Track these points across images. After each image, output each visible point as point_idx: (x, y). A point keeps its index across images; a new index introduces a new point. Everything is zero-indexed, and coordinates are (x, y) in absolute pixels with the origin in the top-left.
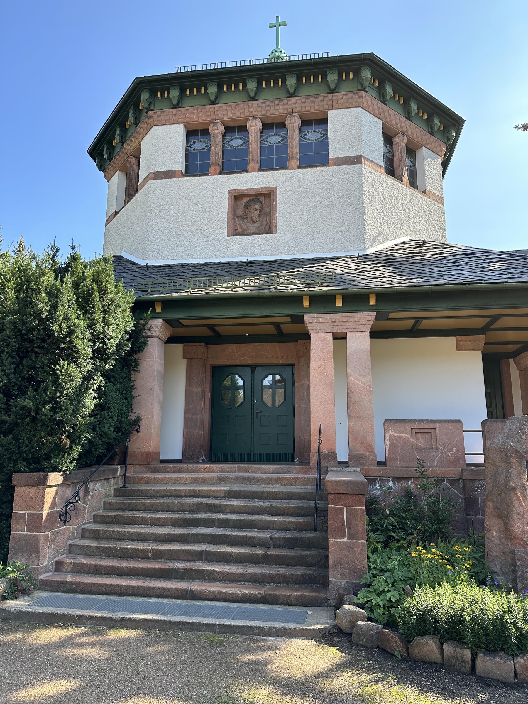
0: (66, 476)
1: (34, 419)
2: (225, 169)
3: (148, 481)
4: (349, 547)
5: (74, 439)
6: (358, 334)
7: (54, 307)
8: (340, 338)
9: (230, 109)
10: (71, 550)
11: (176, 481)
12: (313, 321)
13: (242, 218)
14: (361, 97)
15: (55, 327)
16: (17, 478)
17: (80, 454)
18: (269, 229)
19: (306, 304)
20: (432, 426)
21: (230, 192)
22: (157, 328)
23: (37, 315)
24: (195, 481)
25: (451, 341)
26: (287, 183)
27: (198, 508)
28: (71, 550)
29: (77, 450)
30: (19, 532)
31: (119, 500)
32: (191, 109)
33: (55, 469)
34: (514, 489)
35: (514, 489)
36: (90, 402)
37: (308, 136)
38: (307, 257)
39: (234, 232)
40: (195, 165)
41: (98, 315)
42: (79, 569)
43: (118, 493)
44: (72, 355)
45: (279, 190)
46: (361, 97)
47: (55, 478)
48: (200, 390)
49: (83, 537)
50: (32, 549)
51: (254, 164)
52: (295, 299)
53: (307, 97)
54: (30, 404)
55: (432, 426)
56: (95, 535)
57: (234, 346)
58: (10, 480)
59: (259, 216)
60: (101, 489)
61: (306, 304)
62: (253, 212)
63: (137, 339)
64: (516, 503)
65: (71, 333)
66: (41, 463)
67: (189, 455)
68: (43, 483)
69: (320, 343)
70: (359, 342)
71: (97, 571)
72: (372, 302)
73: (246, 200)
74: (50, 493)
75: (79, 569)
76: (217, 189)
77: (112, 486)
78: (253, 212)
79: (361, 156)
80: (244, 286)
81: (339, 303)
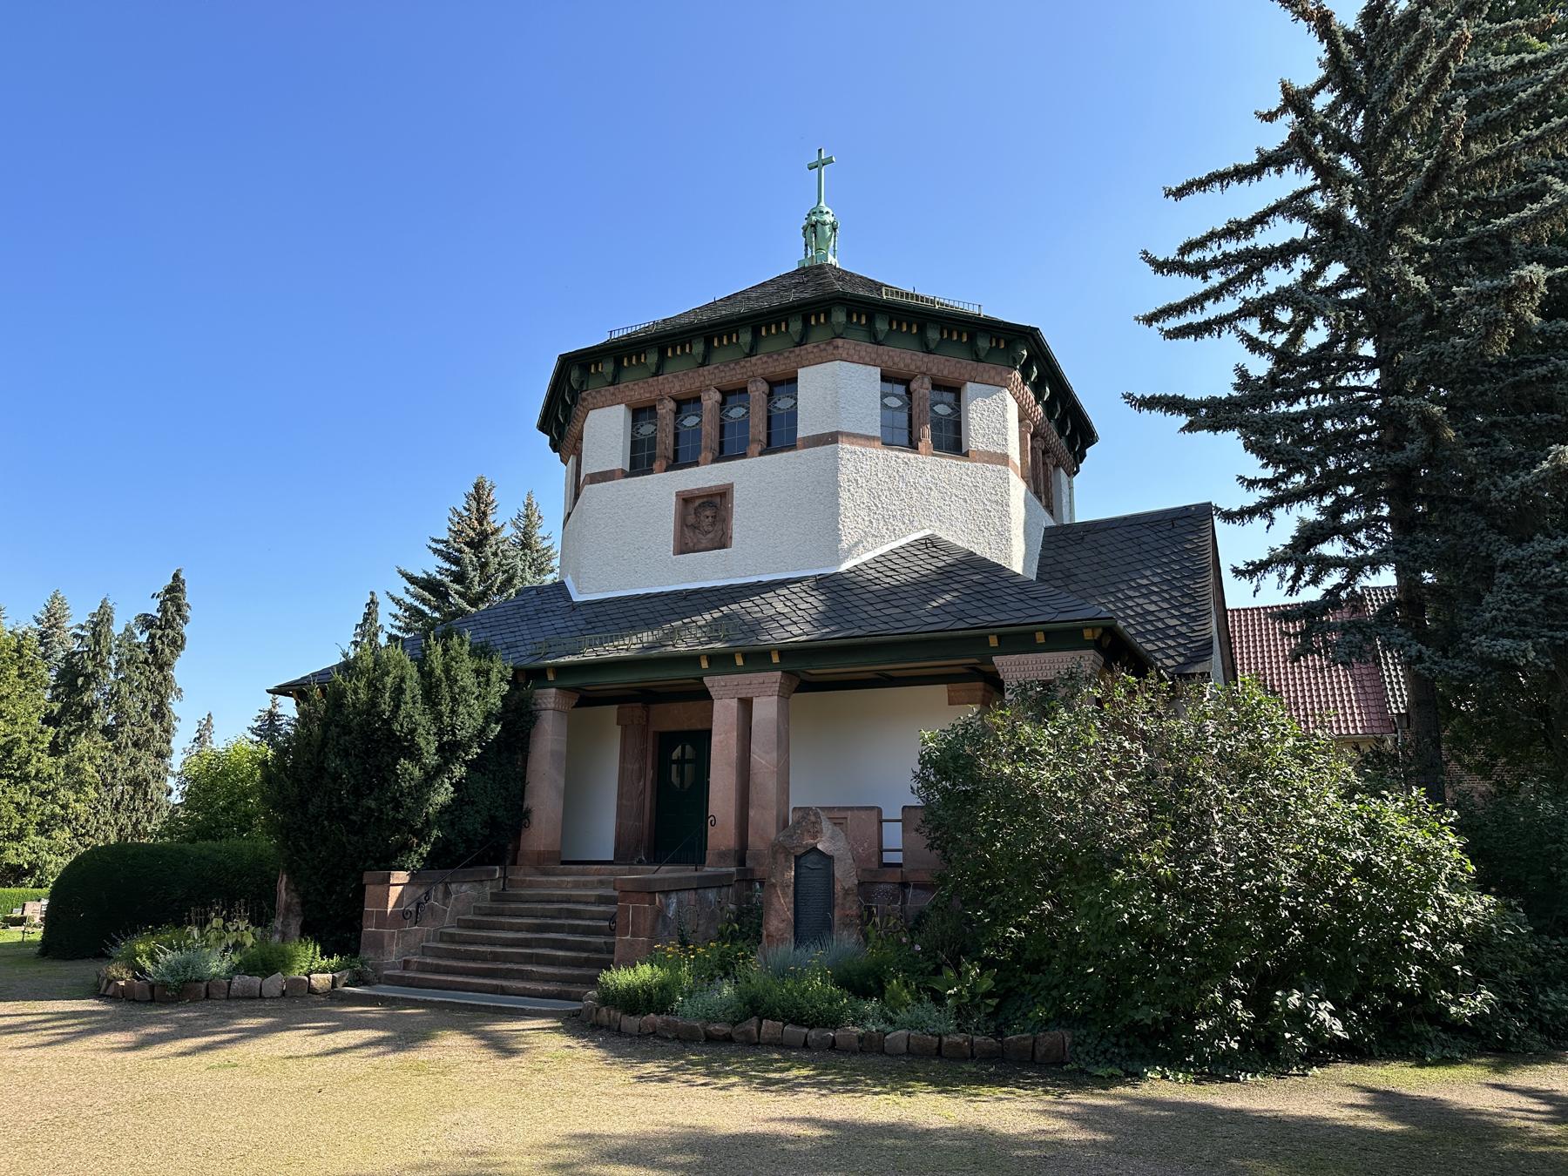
0: (413, 876)
1: (379, 819)
2: (676, 463)
3: (531, 885)
4: (631, 944)
5: (422, 836)
6: (765, 699)
7: (397, 707)
8: (746, 705)
9: (676, 382)
10: (424, 951)
11: (558, 886)
12: (713, 683)
13: (694, 527)
14: (837, 347)
15: (396, 727)
16: (367, 877)
17: (429, 853)
18: (723, 543)
19: (705, 665)
20: (843, 814)
21: (678, 494)
22: (549, 698)
23: (380, 715)
24: (576, 885)
25: (942, 689)
26: (748, 477)
27: (560, 914)
28: (424, 951)
29: (425, 849)
30: (369, 929)
31: (495, 905)
32: (631, 385)
33: (402, 868)
34: (774, 886)
35: (774, 886)
36: (443, 794)
37: (778, 405)
38: (766, 578)
39: (682, 548)
40: (641, 461)
41: (444, 708)
42: (423, 968)
43: (496, 897)
44: (413, 753)
45: (736, 487)
46: (837, 347)
47: (400, 877)
48: (636, 766)
49: (441, 941)
50: (378, 944)
51: (706, 455)
52: (691, 660)
53: (769, 355)
54: (373, 805)
55: (843, 814)
56: (452, 939)
57: (680, 705)
58: (361, 879)
59: (713, 524)
60: (467, 893)
61: (705, 665)
62: (704, 520)
63: (517, 721)
64: (775, 900)
65: (412, 731)
66: (388, 861)
67: (624, 854)
68: (386, 882)
69: (724, 714)
70: (766, 709)
71: (437, 970)
72: (776, 659)
73: (697, 503)
74: (394, 893)
75: (423, 968)
76: (663, 489)
77: (488, 889)
78: (704, 520)
79: (837, 433)
80: (629, 646)
81: (740, 662)
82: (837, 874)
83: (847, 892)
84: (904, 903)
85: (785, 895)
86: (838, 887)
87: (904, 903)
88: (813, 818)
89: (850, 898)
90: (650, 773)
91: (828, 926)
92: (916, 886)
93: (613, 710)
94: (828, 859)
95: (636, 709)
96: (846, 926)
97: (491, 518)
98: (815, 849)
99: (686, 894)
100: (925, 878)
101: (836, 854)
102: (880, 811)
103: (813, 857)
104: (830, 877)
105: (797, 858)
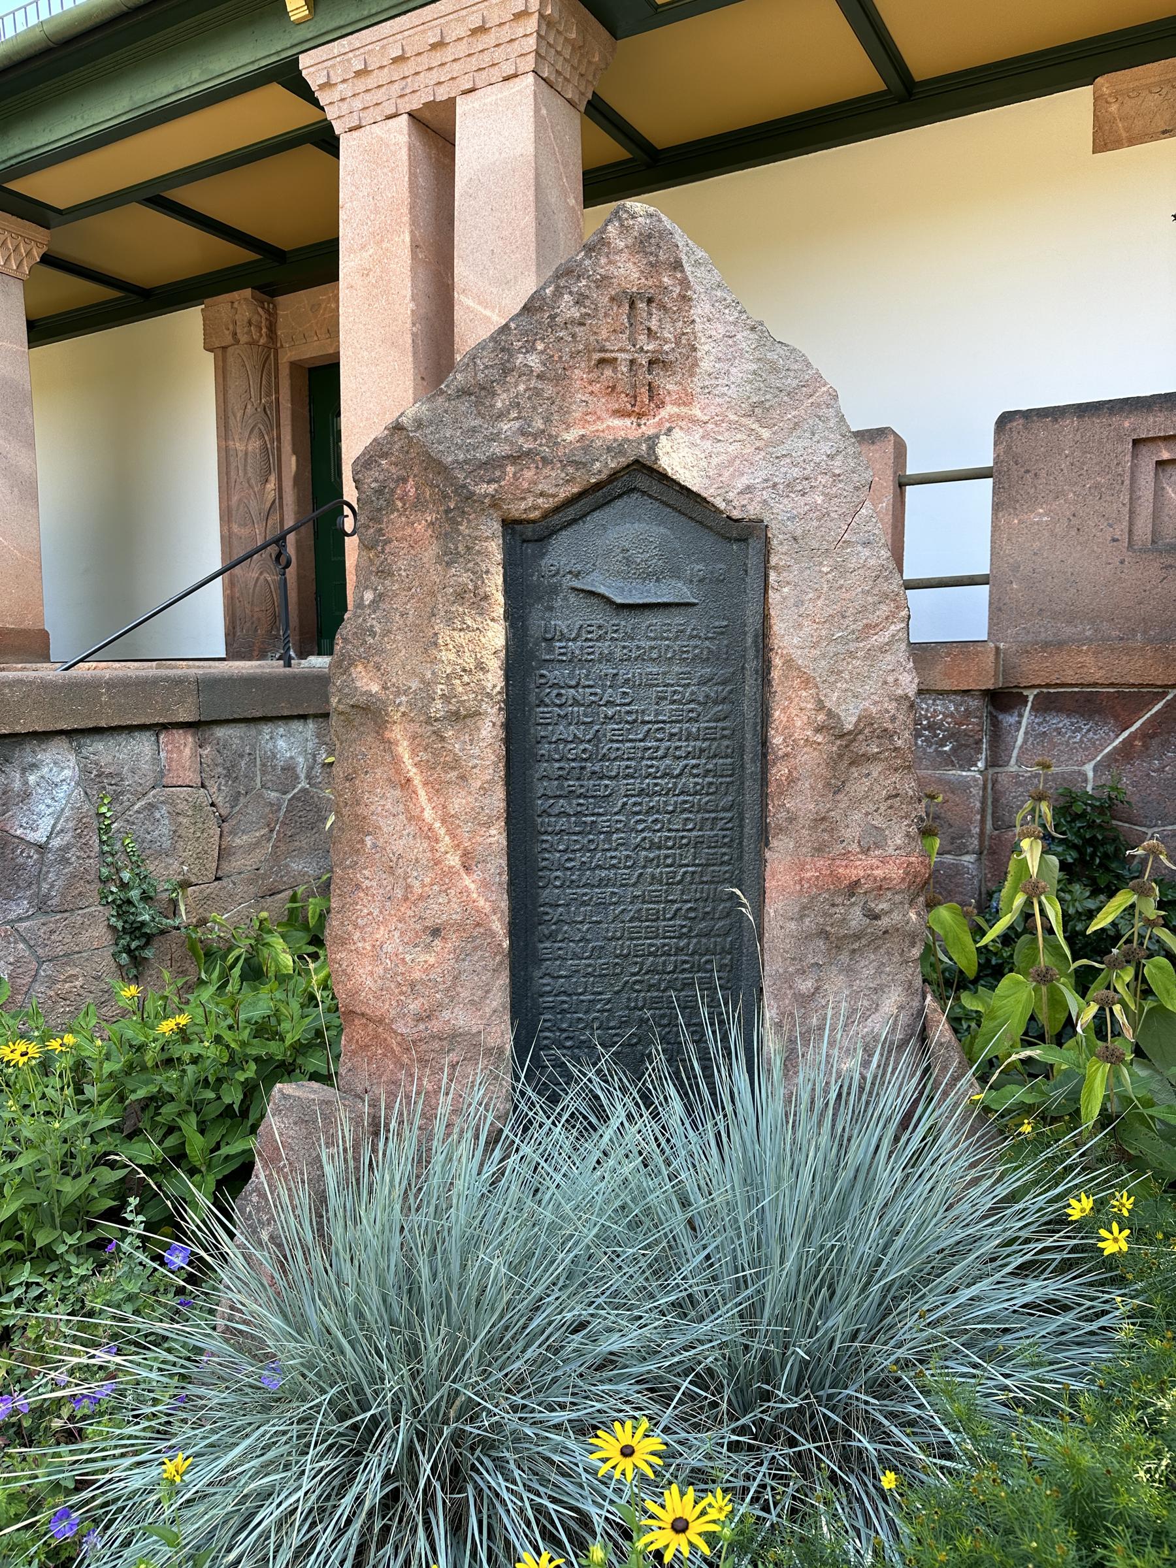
6: (487, 97)
8: (435, 130)
25: (1071, 109)
34: (371, 713)
48: (255, 445)
64: (381, 804)
82: (791, 637)
83: (848, 747)
84: (994, 762)
85: (445, 769)
86: (792, 719)
87: (994, 762)
88: (628, 271)
89: (873, 781)
90: (291, 464)
91: (729, 965)
92: (1049, 703)
93: (190, 321)
94: (733, 542)
95: (239, 305)
96: (839, 944)
97: (962, 964)
98: (639, 479)
99: (135, 754)
100: (1088, 668)
101: (782, 516)
102: (900, 450)
103: (629, 531)
104: (742, 660)
105: (525, 539)
